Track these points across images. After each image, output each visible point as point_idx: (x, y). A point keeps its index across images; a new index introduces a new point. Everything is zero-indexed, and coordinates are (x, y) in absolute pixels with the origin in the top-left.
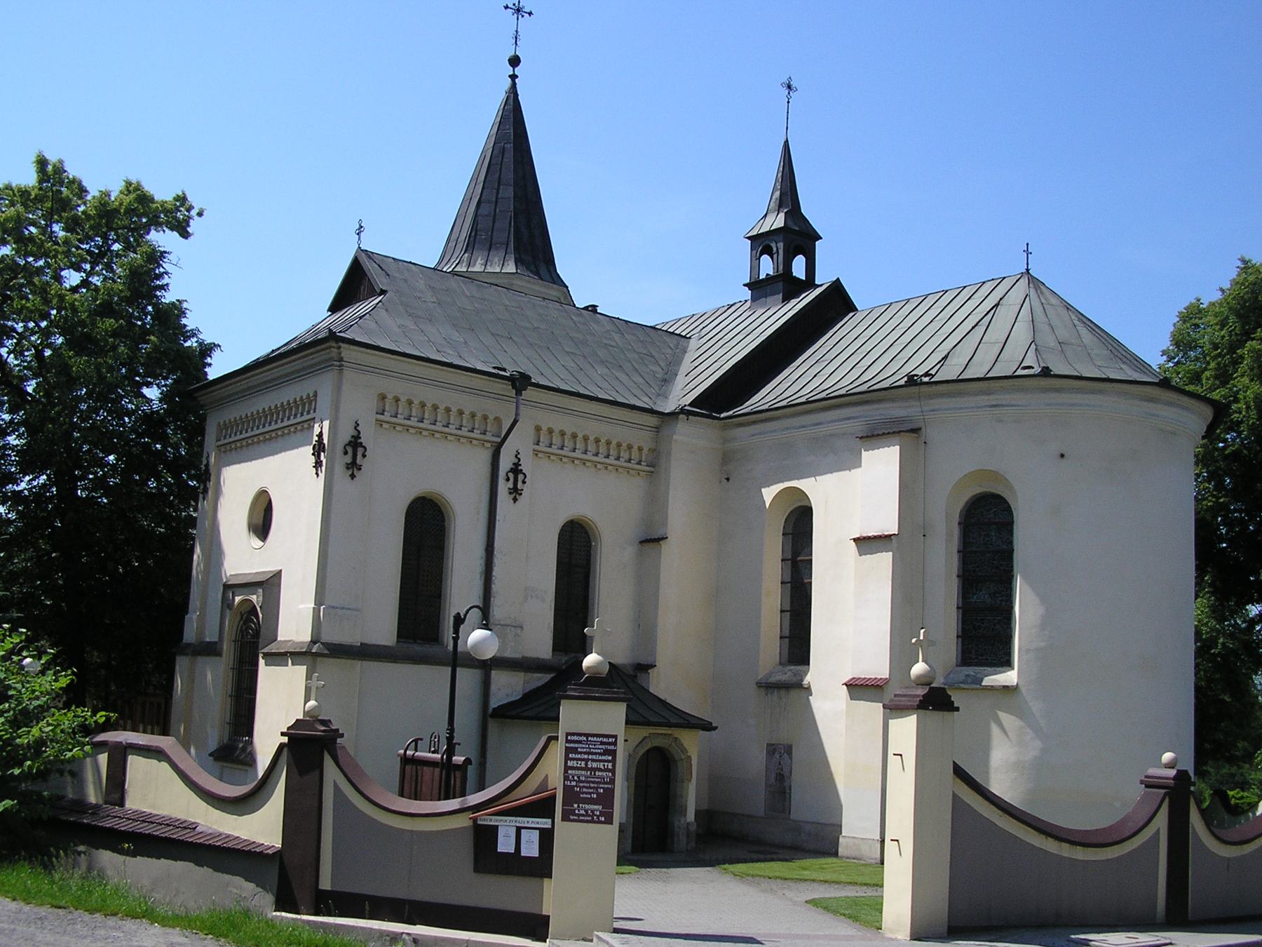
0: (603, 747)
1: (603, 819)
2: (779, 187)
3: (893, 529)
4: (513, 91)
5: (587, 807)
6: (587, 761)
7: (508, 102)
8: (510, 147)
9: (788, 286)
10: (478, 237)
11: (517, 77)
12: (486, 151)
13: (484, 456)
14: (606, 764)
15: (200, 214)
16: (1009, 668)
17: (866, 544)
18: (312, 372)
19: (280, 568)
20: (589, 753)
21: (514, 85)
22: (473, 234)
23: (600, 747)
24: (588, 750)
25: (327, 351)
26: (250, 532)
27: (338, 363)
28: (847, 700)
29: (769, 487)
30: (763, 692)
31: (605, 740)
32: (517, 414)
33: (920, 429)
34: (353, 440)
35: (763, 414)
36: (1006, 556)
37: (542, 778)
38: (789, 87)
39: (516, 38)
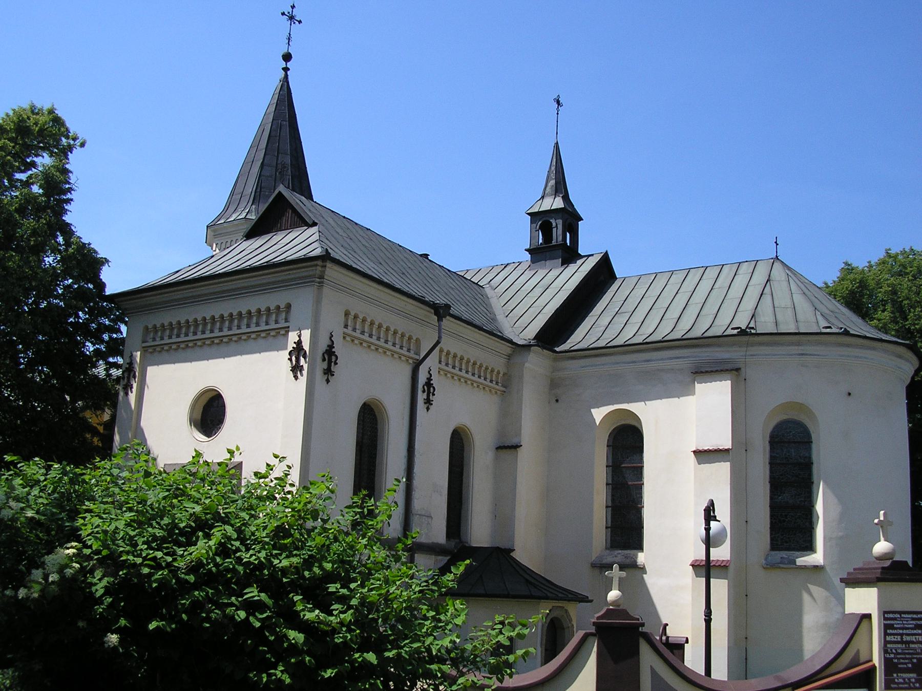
0: (914, 622)
1: (917, 685)
2: (554, 177)
3: (728, 445)
5: (904, 675)
6: (902, 635)
7: (283, 88)
8: (286, 124)
9: (570, 255)
10: (262, 193)
11: (289, 69)
12: (265, 125)
13: (407, 370)
14: (917, 637)
15: (83, 145)
16: (811, 552)
17: (703, 455)
18: (257, 291)
19: (241, 460)
20: (903, 629)
21: (286, 76)
22: (258, 190)
23: (911, 622)
24: (902, 626)
25: (314, 268)
26: (191, 426)
27: (318, 280)
28: (693, 577)
29: (598, 408)
30: (597, 571)
31: (915, 616)
32: (440, 337)
33: (740, 369)
34: (328, 348)
35: (599, 351)
36: (807, 465)
37: (853, 654)
38: (558, 102)
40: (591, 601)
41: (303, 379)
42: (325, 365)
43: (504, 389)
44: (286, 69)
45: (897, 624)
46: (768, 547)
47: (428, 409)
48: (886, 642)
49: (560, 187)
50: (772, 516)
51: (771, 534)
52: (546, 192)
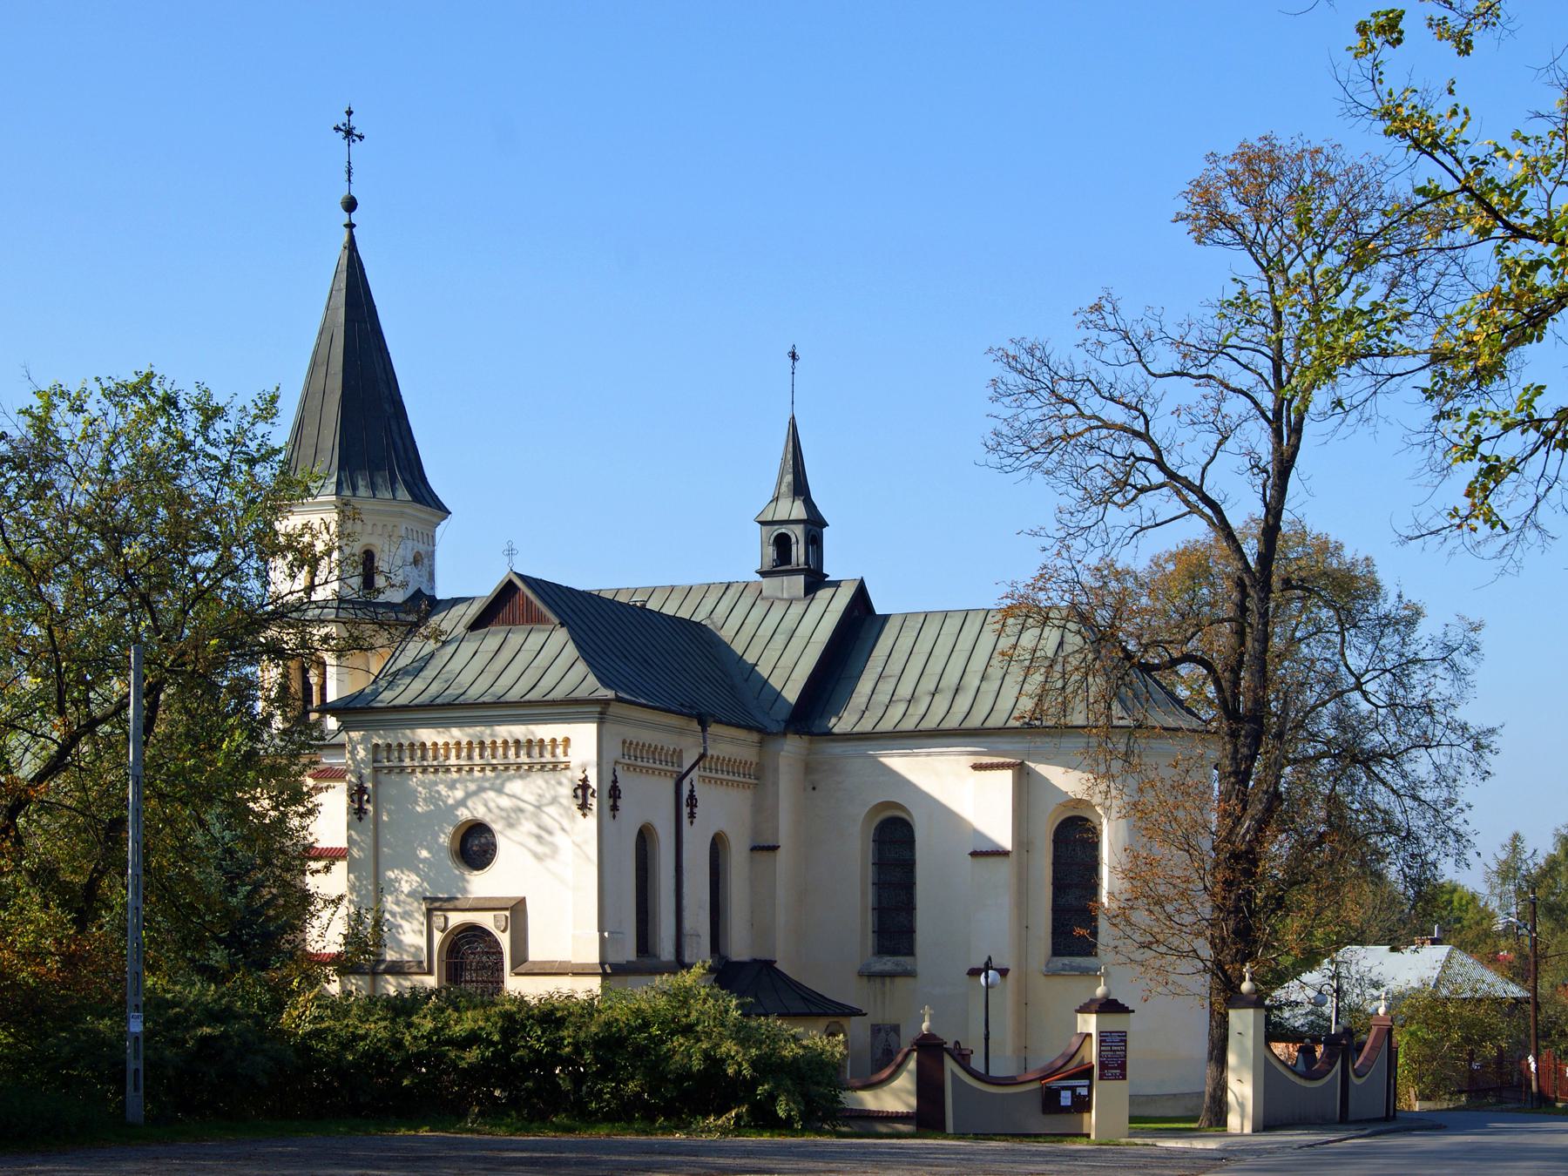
4: (352, 245)
11: (354, 226)
38: (794, 356)
39: (349, 172)
42: (611, 803)
43: (756, 782)
44: (350, 226)
45: (1108, 1039)
46: (1050, 952)
47: (692, 823)
48: (1101, 1051)
49: (800, 488)
50: (1054, 920)
51: (1053, 939)
52: (782, 491)
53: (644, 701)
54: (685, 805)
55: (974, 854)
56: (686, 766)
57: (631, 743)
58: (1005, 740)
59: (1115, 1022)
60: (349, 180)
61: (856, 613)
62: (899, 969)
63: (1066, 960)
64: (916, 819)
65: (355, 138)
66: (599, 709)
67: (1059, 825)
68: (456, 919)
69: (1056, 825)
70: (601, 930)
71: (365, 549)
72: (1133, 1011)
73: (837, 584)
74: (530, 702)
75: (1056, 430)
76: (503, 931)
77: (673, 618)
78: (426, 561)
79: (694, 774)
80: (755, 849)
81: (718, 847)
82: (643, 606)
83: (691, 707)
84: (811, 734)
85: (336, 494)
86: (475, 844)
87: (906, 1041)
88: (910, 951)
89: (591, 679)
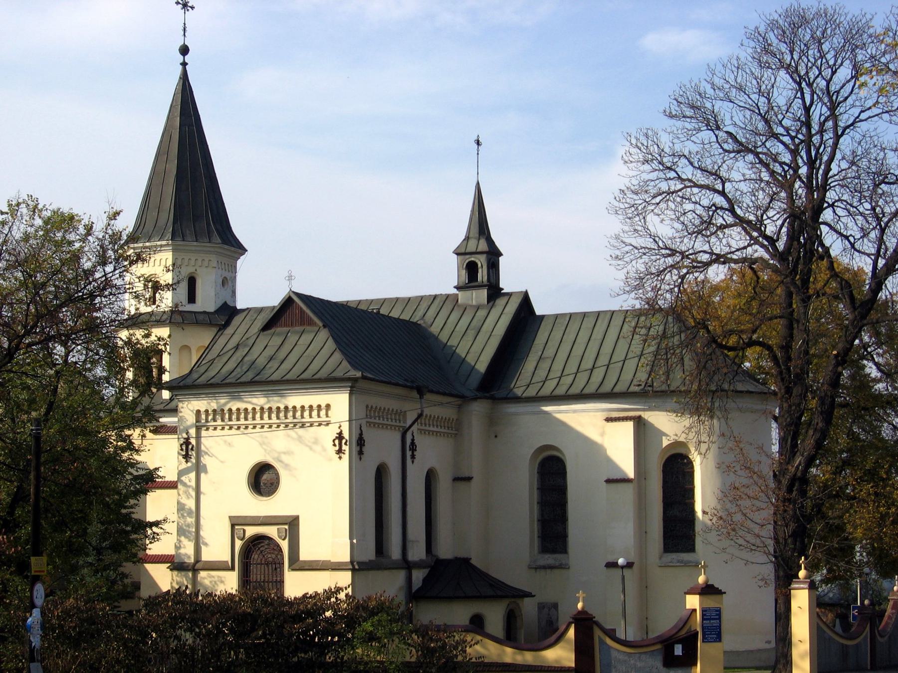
4: (185, 77)
11: (187, 64)
38: (478, 143)
40: (534, 596)
41: (346, 457)
43: (456, 432)
46: (662, 550)
47: (413, 462)
50: (664, 527)
53: (369, 375)
54: (408, 450)
55: (608, 481)
56: (409, 422)
57: (372, 407)
58: (521, 405)
59: (712, 602)
60: (184, 35)
61: (523, 315)
62: (557, 564)
63: (674, 556)
64: (567, 458)
65: (189, 8)
66: (350, 385)
67: (666, 460)
68: (251, 531)
69: (664, 460)
70: (351, 538)
71: (190, 275)
72: (725, 593)
73: (510, 295)
74: (303, 380)
75: (664, 186)
76: (284, 540)
77: (398, 320)
78: (230, 282)
79: (415, 428)
80: (456, 479)
81: (430, 477)
82: (378, 312)
83: (412, 382)
84: (493, 398)
85: (171, 240)
86: (266, 477)
87: (565, 615)
88: (691, 549)
89: (345, 363)
